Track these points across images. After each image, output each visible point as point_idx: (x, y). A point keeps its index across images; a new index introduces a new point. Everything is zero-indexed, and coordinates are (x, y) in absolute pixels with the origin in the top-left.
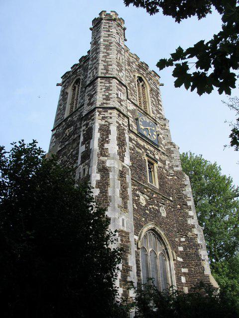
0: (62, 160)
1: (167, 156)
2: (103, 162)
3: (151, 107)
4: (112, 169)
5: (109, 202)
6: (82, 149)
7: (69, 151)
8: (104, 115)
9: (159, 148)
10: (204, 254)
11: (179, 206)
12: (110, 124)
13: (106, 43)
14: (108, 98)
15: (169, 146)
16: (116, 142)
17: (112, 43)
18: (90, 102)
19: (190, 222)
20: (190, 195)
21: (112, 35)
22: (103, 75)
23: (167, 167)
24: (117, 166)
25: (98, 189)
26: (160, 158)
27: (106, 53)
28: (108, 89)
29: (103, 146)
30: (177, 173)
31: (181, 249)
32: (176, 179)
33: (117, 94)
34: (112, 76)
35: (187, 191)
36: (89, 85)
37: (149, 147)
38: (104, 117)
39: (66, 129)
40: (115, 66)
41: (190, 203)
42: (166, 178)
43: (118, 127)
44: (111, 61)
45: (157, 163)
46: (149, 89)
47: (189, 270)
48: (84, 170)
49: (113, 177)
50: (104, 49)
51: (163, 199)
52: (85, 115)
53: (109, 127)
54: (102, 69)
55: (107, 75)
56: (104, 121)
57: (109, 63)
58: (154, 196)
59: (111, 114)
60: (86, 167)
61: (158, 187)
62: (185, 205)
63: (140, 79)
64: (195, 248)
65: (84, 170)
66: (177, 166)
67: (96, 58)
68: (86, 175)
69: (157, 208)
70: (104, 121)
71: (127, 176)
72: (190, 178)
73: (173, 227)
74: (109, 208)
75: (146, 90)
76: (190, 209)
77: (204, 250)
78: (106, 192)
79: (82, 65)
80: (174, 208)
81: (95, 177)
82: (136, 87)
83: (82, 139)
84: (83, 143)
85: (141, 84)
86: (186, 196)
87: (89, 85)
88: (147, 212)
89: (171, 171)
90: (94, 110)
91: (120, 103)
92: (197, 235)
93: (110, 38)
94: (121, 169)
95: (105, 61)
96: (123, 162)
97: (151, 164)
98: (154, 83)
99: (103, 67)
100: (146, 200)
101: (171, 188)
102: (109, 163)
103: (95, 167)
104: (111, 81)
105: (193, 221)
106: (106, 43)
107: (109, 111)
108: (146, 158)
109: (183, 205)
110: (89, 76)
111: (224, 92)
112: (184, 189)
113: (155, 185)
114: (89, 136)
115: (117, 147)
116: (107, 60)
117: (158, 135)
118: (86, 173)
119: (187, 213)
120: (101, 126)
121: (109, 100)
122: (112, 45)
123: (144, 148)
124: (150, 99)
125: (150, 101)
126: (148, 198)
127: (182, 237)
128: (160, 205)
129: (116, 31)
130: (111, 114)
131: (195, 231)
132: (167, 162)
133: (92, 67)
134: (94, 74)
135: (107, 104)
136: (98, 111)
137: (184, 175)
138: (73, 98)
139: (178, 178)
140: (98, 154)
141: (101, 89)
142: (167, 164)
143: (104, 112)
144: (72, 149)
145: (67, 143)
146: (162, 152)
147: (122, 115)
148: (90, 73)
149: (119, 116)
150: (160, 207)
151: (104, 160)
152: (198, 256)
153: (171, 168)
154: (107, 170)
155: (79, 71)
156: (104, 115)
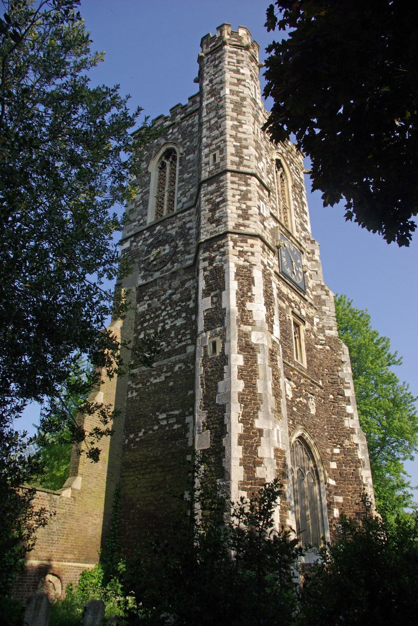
0: (149, 305)
1: (316, 309)
2: (247, 335)
3: (294, 218)
4: (261, 347)
5: (258, 404)
6: (205, 304)
7: (165, 291)
8: (242, 247)
9: (306, 297)
10: (367, 476)
11: (331, 396)
12: (252, 265)
13: (235, 98)
14: (245, 215)
15: (319, 292)
16: (263, 300)
17: (243, 99)
18: (213, 216)
19: (348, 423)
20: (349, 380)
21: (244, 80)
22: (234, 168)
23: (315, 328)
24: (266, 343)
25: (242, 381)
26: (307, 314)
27: (236, 119)
28: (245, 197)
29: (244, 305)
30: (329, 339)
31: (333, 465)
32: (328, 350)
33: (259, 208)
34: (249, 171)
35: (345, 371)
36: (209, 181)
37: (294, 295)
38: (242, 252)
39: (153, 246)
40: (252, 150)
41: (349, 393)
42: (314, 347)
43: (264, 272)
44: (246, 139)
45: (304, 324)
46: (290, 184)
47: (344, 499)
48: (214, 344)
49: (262, 359)
50: (233, 110)
51: (312, 386)
52: (206, 241)
53: (251, 272)
54: (232, 154)
55: (242, 169)
56: (243, 259)
57: (244, 143)
58: (302, 381)
59: (252, 246)
60: (218, 340)
61: (305, 365)
62: (341, 395)
63: (279, 164)
64: (354, 465)
65: (214, 344)
66: (331, 329)
67: (218, 126)
68: (218, 354)
69: (305, 401)
70: (243, 259)
71: (278, 357)
72: (350, 351)
73: (323, 430)
74: (260, 414)
75: (285, 185)
76: (348, 401)
77: (367, 469)
78: (254, 386)
79: (179, 124)
80: (324, 399)
81: (236, 360)
82: (274, 183)
83: (202, 285)
84: (206, 294)
85: (279, 173)
86: (343, 381)
87: (209, 181)
88: (295, 409)
89: (321, 337)
90: (224, 235)
91: (263, 224)
92: (357, 445)
93: (241, 88)
94: (271, 348)
95: (235, 138)
96: (272, 333)
97: (296, 325)
98: (296, 168)
99: (233, 150)
100: (293, 391)
101: (321, 365)
102: (255, 338)
103: (234, 344)
104: (249, 181)
105: (351, 423)
106: (235, 98)
107: (250, 241)
108: (291, 317)
109: (338, 394)
110: (204, 160)
111: (280, 43)
112: (340, 368)
113: (302, 362)
114: (217, 283)
115: (264, 308)
116: (239, 135)
117: (305, 272)
118: (219, 350)
119: (344, 409)
120: (239, 267)
121: (248, 219)
122: (245, 103)
123: (288, 299)
124: (292, 202)
125: (293, 207)
126: (295, 386)
127: (335, 447)
128: (309, 395)
129: (249, 73)
130: (252, 246)
131: (356, 439)
132: (316, 320)
133: (211, 145)
134: (218, 160)
135: (244, 226)
136: (232, 240)
137: (341, 344)
138: (161, 186)
139: (331, 348)
140: (238, 320)
141: (234, 196)
142: (315, 324)
143: (242, 241)
144: (170, 287)
145: (157, 275)
146: (310, 304)
147: (266, 247)
148: (207, 156)
149: (264, 249)
150: (308, 399)
151: (247, 331)
152: (357, 478)
153: (322, 330)
154: (253, 349)
155: (172, 133)
156: (242, 247)
